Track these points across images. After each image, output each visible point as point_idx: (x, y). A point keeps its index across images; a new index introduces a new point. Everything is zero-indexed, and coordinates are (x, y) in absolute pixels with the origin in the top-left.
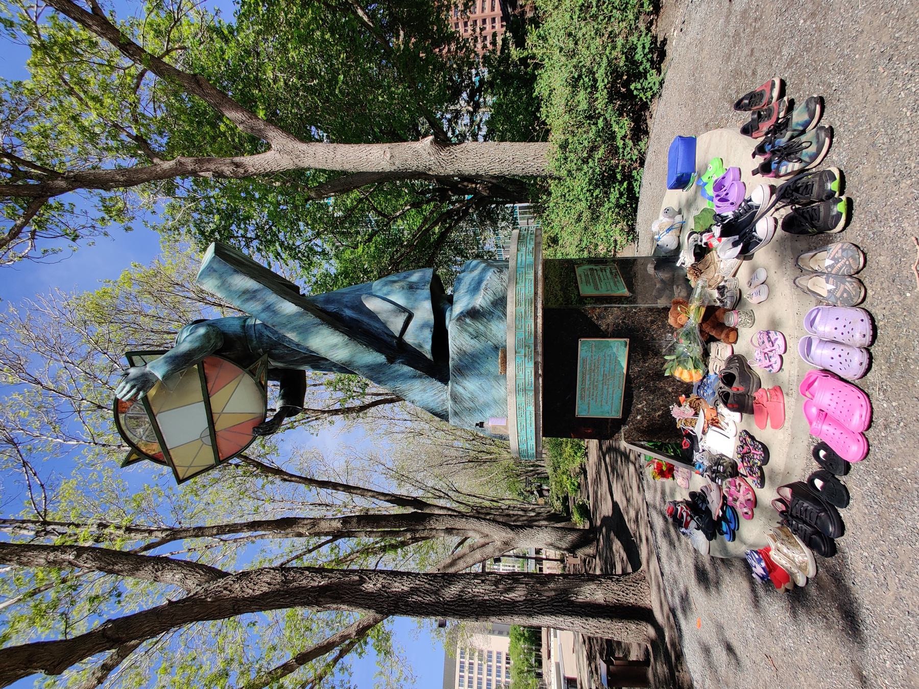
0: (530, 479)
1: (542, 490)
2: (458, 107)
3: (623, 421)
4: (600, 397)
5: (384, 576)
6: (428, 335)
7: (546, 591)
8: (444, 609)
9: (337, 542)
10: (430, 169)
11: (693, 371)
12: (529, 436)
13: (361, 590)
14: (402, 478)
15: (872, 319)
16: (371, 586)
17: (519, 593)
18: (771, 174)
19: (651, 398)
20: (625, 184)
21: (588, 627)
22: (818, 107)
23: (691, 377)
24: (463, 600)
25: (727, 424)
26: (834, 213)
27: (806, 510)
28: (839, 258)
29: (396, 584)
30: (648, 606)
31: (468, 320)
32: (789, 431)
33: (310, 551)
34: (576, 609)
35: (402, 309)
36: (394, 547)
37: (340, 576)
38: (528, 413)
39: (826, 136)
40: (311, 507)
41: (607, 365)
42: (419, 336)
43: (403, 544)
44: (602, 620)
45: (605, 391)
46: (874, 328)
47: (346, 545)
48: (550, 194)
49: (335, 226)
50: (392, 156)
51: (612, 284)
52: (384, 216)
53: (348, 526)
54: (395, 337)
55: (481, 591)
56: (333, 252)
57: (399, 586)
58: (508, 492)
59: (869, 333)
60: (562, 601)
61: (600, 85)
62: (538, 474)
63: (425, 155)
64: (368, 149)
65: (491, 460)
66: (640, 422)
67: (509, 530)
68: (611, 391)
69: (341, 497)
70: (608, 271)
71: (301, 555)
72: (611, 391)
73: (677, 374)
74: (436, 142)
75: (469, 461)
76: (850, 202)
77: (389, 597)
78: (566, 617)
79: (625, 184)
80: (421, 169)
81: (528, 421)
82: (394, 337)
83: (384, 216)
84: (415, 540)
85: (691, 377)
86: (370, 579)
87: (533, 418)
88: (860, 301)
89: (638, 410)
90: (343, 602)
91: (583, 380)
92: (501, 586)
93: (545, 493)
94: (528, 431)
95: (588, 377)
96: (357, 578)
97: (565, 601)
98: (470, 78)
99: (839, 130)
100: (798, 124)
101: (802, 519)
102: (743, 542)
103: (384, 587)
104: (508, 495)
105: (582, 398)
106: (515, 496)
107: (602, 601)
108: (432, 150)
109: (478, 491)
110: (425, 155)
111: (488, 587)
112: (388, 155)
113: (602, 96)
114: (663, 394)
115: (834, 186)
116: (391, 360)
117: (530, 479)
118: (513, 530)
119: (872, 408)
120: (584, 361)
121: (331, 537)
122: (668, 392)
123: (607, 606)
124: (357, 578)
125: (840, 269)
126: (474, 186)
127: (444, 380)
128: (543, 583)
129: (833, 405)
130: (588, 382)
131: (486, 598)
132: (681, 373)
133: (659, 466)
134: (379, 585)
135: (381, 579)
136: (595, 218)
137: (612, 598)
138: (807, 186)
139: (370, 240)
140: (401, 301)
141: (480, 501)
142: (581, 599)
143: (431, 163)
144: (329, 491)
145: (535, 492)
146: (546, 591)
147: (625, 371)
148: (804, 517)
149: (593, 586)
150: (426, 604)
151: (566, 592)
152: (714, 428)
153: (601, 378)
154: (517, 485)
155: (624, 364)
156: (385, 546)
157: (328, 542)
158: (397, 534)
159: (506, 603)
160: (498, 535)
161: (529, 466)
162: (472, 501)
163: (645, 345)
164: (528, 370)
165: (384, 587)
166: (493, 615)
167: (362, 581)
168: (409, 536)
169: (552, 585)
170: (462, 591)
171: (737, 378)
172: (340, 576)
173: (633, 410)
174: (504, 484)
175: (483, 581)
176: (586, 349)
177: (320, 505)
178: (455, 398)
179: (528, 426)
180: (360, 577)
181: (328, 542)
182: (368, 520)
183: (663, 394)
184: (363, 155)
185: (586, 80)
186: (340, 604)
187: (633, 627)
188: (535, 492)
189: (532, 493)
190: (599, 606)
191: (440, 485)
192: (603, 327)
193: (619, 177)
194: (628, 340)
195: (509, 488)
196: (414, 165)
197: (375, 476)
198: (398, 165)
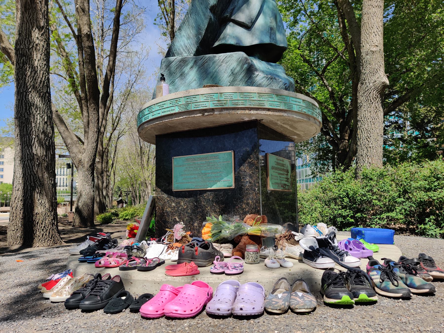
0: (131, 195)
1: (123, 203)
2: (408, 128)
3: (169, 192)
4: (189, 172)
5: (45, 46)
6: (232, 41)
7: (42, 170)
8: (23, 93)
9: (73, 39)
10: (362, 84)
11: (210, 234)
12: (155, 113)
13: (33, 27)
14: (127, 95)
15: (255, 317)
16: (37, 36)
17: (39, 150)
18: (369, 267)
19: (189, 211)
20: (353, 220)
21: (16, 201)
22: (427, 290)
23: (205, 233)
24: (30, 107)
25: (169, 254)
26: (340, 294)
27: (102, 289)
28: (304, 299)
29: (39, 56)
30: (34, 245)
31: (246, 66)
32: (164, 280)
33: (65, 17)
34: (29, 192)
35: (253, 22)
36: (73, 84)
37: (43, 10)
38: (173, 108)
39: (404, 294)
40: (101, 24)
41: (213, 175)
42: (232, 33)
43: (76, 92)
44: (22, 212)
45: (193, 176)
46: (248, 317)
47: (72, 46)
48: (344, 171)
49: (315, 32)
50: (373, 52)
51: (277, 181)
52: (324, 71)
53: (85, 41)
54: (231, 15)
55: (38, 121)
56: (295, 31)
57: (37, 59)
58: (119, 179)
59: (244, 313)
60: (34, 182)
61: (431, 194)
62: (134, 201)
63: (374, 78)
64: (380, 33)
65: (142, 165)
66: (170, 206)
67: (90, 163)
68: (192, 180)
69: (107, 46)
70: (286, 183)
71: (62, 10)
72: (192, 180)
73: (207, 224)
74: (385, 86)
75: (141, 147)
76: (349, 306)
77: (29, 49)
78: (22, 185)
79: (353, 220)
80: (363, 77)
81: (166, 110)
82: (231, 14)
83: (324, 71)
84: (80, 100)
85: (205, 233)
86: (42, 35)
87: (169, 113)
88: (270, 310)
89: (179, 203)
90: (22, 14)
91: (201, 159)
92: (43, 136)
93: (121, 205)
94: (160, 111)
95: (204, 161)
96: (42, 24)
97: (35, 184)
98: (430, 137)
99: (409, 302)
100: (412, 280)
101: (95, 287)
102: (77, 266)
103: (37, 45)
104: (118, 179)
105: (187, 160)
106: (117, 183)
107: (36, 211)
108: (378, 84)
109: (120, 156)
110: (374, 78)
111: (41, 126)
112: (374, 49)
113: (422, 196)
114: (192, 219)
115: (363, 296)
116: (213, 9)
117: (131, 195)
118: (90, 166)
119: (183, 319)
120: (216, 157)
121: (77, 34)
122: (194, 222)
123: (33, 215)
124: (42, 24)
125: (295, 300)
126: (347, 138)
127: (198, 53)
128: (47, 168)
129: (185, 296)
130: (199, 162)
131: (33, 125)
132: (208, 227)
133: (137, 228)
134: (37, 42)
135: (42, 43)
136: (327, 203)
137: (38, 219)
138: (362, 282)
139: (306, 61)
140: (261, 21)
141: (112, 156)
142: (37, 196)
143: (368, 84)
144: (112, 27)
145: (121, 198)
146: (42, 170)
147: (209, 188)
148: (97, 288)
149: (47, 205)
150: (25, 79)
151: (42, 185)
152: (166, 248)
153: (203, 172)
154: (125, 185)
155: (214, 187)
156: (74, 78)
157: (73, 32)
158: (83, 86)
159: (30, 140)
160: (85, 155)
161: (139, 194)
162: (112, 149)
163: (228, 202)
164: (207, 104)
165: (37, 45)
166: (20, 130)
167: (40, 29)
168: (82, 95)
169: (46, 175)
170: (37, 107)
171: (205, 251)
172: (43, 10)
173: (179, 200)
174: (125, 175)
175: (46, 123)
176: (225, 158)
177: (102, 30)
178: (184, 62)
179: (163, 110)
180: (43, 27)
181: (73, 32)
182: (90, 59)
183: (192, 219)
184: (375, 30)
185: (436, 184)
186: (22, 11)
187: (19, 234)
188: (121, 198)
189: (120, 196)
190: (32, 209)
191: (122, 126)
192: (242, 168)
193: (359, 215)
194: (233, 187)
195: (122, 179)
196: (366, 70)
197: (127, 76)
198: (365, 57)
